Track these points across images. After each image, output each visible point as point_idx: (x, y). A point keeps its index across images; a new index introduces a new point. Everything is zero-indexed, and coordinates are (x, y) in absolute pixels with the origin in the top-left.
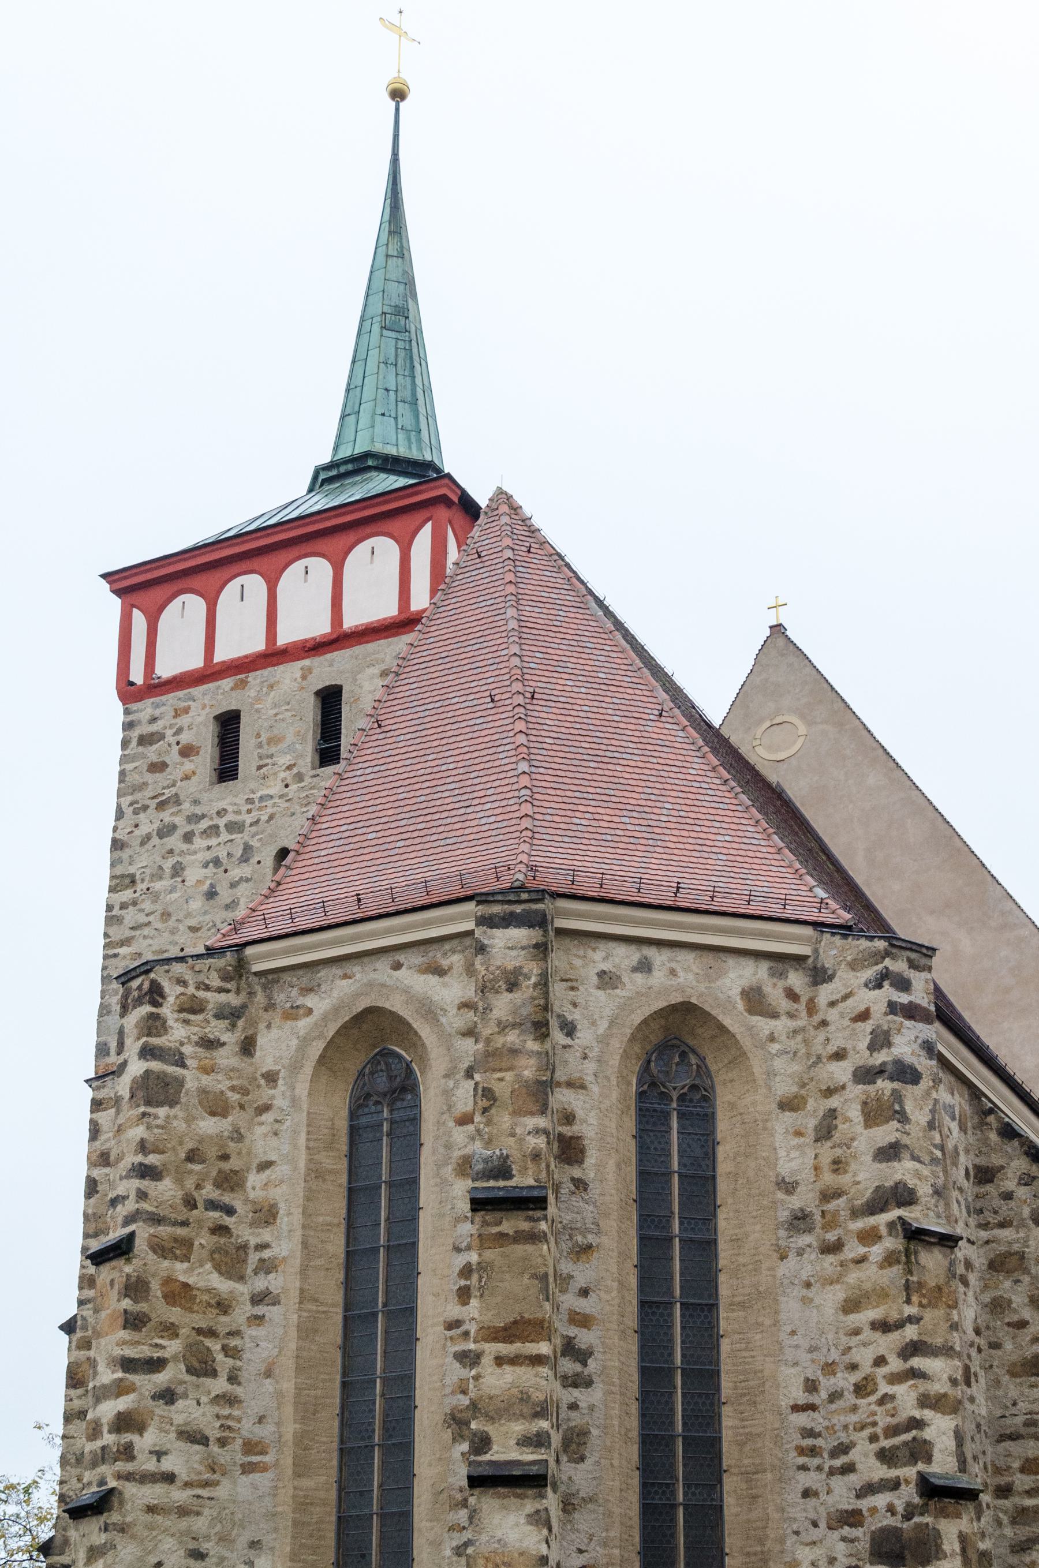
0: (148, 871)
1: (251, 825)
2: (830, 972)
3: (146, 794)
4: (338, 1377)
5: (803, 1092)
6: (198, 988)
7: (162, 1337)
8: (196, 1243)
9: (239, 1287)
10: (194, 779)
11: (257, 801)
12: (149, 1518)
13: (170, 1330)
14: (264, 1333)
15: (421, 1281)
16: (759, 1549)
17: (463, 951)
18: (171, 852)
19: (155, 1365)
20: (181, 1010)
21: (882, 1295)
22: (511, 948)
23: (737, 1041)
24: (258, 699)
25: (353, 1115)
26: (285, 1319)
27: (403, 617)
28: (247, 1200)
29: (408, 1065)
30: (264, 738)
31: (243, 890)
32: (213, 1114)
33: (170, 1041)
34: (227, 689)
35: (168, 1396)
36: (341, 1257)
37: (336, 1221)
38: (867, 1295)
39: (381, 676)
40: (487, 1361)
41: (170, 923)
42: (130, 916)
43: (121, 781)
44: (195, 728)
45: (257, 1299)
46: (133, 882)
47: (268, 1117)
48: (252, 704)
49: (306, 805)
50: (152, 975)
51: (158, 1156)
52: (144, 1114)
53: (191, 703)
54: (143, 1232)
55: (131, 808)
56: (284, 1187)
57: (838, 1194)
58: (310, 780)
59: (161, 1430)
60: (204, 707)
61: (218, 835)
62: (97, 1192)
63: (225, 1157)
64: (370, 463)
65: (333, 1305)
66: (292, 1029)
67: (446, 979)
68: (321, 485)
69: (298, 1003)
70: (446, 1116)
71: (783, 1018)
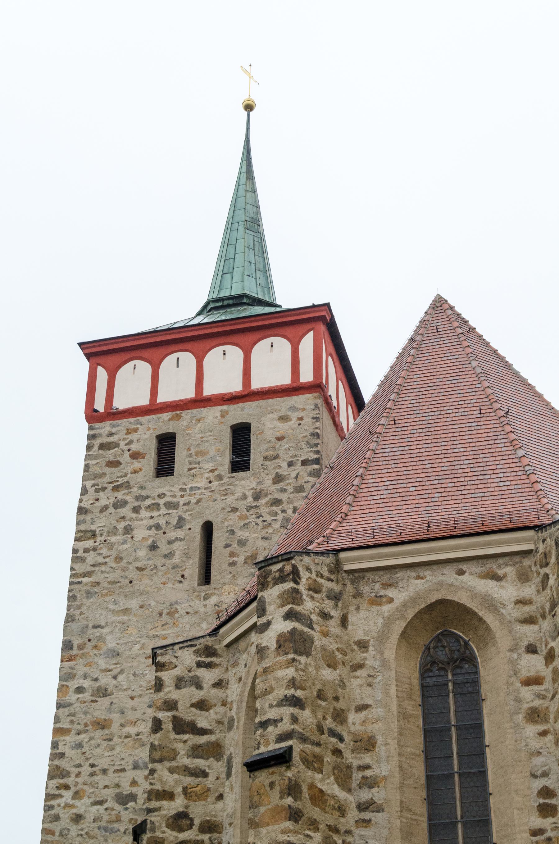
0: (106, 529)
1: (184, 505)
3: (104, 480)
6: (317, 575)
7: (310, 829)
8: (325, 760)
9: (351, 798)
10: (141, 473)
11: (188, 490)
14: (371, 833)
15: (492, 800)
17: (514, 565)
18: (123, 518)
26: (390, 823)
27: (295, 385)
29: (466, 643)
30: (193, 451)
31: (177, 546)
32: (329, 666)
33: (305, 610)
34: (166, 419)
36: (423, 780)
39: (279, 419)
41: (122, 564)
42: (91, 558)
43: (85, 471)
44: (142, 442)
45: (363, 807)
46: (94, 535)
48: (184, 430)
49: (225, 495)
50: (293, 562)
51: (302, 692)
52: (294, 660)
53: (138, 426)
55: (94, 488)
58: (228, 480)
60: (149, 429)
61: (159, 510)
62: (162, 729)
63: (336, 699)
66: (378, 611)
67: (502, 583)
69: (381, 594)
70: (513, 679)
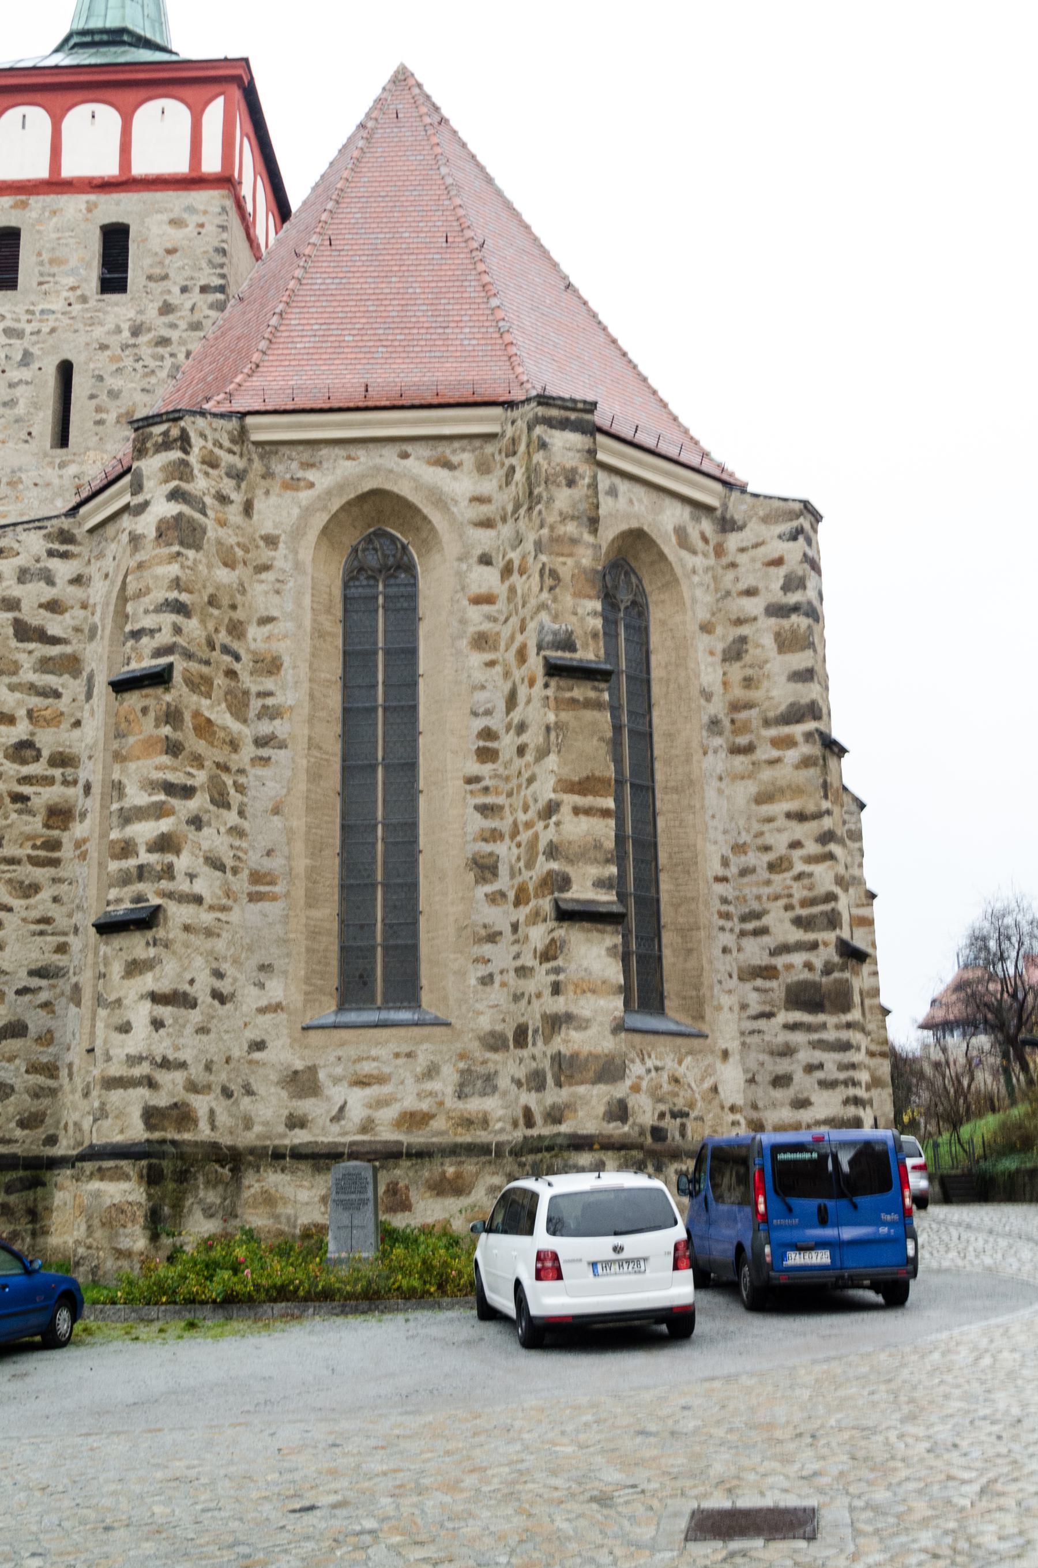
2: (740, 523)
4: (338, 820)
5: (713, 620)
6: (214, 445)
12: (184, 936)
13: (198, 760)
16: (694, 993)
19: (187, 792)
20: (203, 462)
21: (798, 791)
22: (569, 449)
23: (672, 569)
24: (39, 221)
25: (346, 586)
28: (248, 650)
30: (45, 256)
35: (196, 822)
37: (334, 679)
38: (782, 791)
40: (566, 810)
45: (261, 742)
47: (268, 576)
48: (33, 225)
50: (182, 423)
52: (178, 554)
54: (180, 665)
56: (288, 642)
57: (749, 706)
59: (193, 854)
64: (126, 38)
65: (333, 755)
67: (457, 473)
68: (73, 48)
71: (700, 555)
